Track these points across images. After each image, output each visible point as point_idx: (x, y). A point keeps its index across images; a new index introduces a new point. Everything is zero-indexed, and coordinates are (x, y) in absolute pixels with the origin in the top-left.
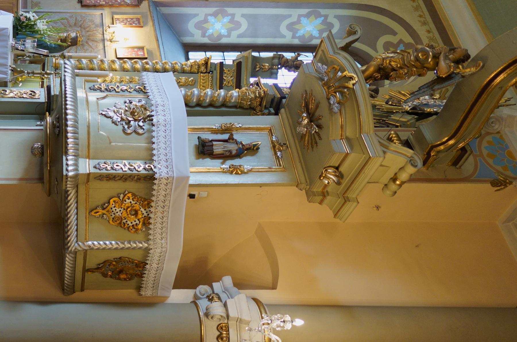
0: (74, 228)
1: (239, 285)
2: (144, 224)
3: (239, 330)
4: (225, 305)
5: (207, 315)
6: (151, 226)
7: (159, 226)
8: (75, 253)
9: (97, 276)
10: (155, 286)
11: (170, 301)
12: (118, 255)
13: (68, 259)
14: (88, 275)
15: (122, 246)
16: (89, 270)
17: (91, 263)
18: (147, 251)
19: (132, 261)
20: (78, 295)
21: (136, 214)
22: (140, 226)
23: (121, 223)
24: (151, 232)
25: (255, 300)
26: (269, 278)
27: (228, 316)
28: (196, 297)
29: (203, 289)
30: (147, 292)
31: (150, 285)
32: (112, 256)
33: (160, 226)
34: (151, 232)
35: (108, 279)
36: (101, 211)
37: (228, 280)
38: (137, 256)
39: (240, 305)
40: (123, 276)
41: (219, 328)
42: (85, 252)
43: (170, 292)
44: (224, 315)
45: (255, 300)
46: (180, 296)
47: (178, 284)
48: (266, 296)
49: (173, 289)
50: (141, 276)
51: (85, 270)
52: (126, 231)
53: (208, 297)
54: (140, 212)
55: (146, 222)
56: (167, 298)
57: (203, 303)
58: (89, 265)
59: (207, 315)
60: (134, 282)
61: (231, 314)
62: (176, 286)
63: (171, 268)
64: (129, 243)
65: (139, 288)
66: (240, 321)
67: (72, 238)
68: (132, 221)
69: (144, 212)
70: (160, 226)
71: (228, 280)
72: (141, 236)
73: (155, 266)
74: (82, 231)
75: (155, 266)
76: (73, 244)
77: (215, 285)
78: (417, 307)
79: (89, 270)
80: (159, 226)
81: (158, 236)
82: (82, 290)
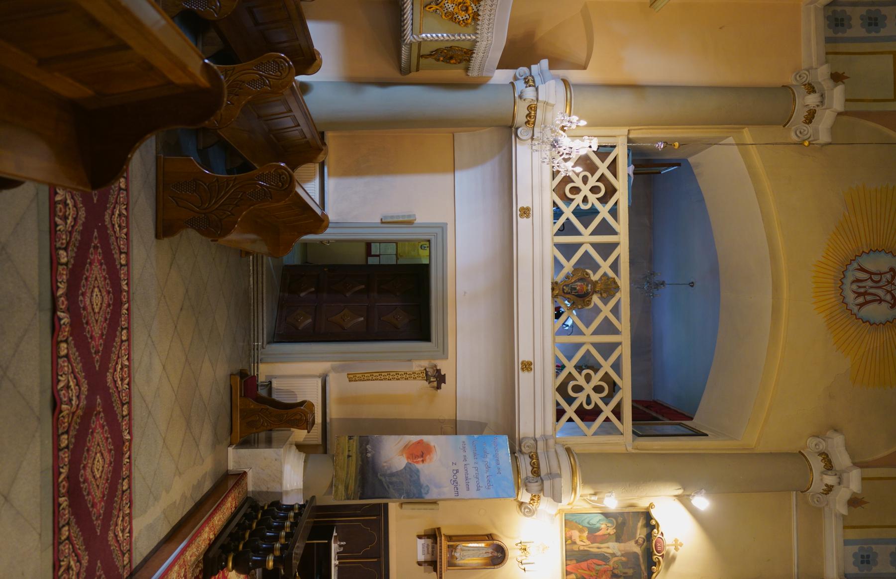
0: (410, 22)
1: (555, 63)
2: (474, 19)
3: (545, 111)
4: (537, 89)
5: (520, 97)
6: (479, 22)
7: (486, 22)
8: (411, 44)
9: (430, 61)
10: (481, 68)
11: (492, 82)
12: (449, 45)
13: (404, 50)
14: (422, 61)
15: (452, 38)
16: (422, 56)
17: (425, 51)
18: (475, 42)
19: (461, 50)
20: (414, 75)
21: (467, 10)
22: (469, 21)
23: (452, 18)
24: (479, 27)
25: (565, 81)
26: (583, 56)
27: (537, 99)
28: (516, 78)
29: (523, 70)
30: (474, 73)
31: (477, 68)
32: (442, 46)
33: (487, 22)
34: (479, 27)
35: (440, 63)
36: (435, 7)
37: (545, 63)
38: (467, 46)
39: (550, 91)
40: (452, 62)
41: (530, 108)
42: (420, 44)
43: (494, 72)
44: (535, 99)
45: (565, 81)
46: (502, 76)
47: (502, 65)
48: (575, 76)
49: (498, 68)
50: (469, 61)
51: (420, 56)
52: (457, 25)
53: (525, 79)
54: (470, 8)
55: (476, 16)
56: (490, 78)
57: (520, 85)
58: (422, 52)
59: (520, 97)
60: (464, 64)
61: (540, 99)
62: (500, 67)
63: (496, 55)
64: (459, 35)
65: (467, 69)
66: (546, 103)
67: (408, 27)
68: (462, 16)
69: (474, 7)
70: (487, 22)
71: (545, 63)
72: (470, 29)
73: (481, 54)
74: (417, 25)
75: (481, 54)
76: (409, 37)
77: (534, 67)
78: (787, 454)
79: (422, 56)
80: (486, 22)
81: (485, 31)
82: (417, 70)
